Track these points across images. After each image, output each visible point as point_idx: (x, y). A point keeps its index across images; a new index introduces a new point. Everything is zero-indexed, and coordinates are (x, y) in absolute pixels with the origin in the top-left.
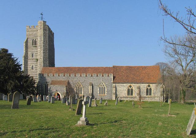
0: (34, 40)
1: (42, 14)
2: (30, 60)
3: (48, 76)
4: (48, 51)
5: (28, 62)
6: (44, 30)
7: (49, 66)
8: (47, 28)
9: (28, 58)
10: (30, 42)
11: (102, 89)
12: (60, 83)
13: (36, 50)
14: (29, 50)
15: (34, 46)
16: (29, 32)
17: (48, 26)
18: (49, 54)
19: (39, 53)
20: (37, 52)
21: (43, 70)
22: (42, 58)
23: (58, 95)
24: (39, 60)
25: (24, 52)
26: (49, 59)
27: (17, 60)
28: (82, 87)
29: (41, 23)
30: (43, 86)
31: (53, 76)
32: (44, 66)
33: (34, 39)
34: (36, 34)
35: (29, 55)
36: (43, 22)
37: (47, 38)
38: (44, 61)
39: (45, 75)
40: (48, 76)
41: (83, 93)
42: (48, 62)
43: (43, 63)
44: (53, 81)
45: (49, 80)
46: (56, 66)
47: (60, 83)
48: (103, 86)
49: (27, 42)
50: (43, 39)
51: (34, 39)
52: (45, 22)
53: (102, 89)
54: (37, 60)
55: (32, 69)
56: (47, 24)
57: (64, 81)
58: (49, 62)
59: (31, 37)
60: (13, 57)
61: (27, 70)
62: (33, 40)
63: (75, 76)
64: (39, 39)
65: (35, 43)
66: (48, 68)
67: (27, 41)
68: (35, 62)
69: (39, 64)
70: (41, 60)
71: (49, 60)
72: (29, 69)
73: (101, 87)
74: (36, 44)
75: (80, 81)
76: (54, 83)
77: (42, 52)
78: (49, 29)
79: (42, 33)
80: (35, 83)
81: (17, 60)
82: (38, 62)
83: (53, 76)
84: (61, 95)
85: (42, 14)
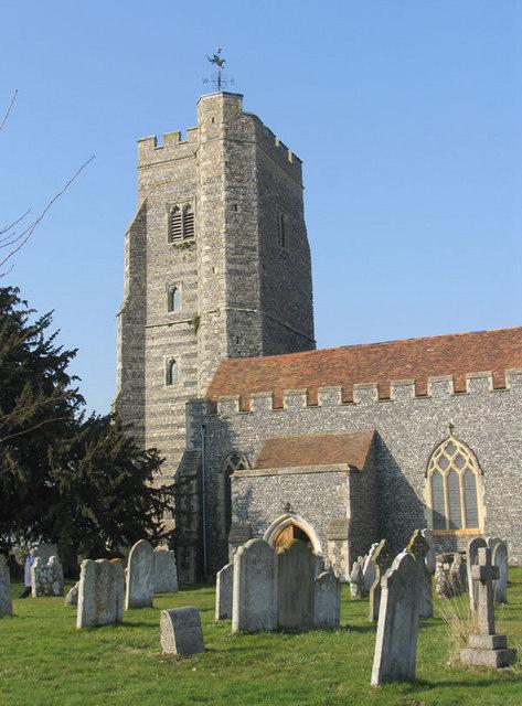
0: (181, 212)
1: (217, 61)
2: (157, 330)
3: (244, 411)
4: (256, 264)
5: (149, 343)
6: (233, 140)
7: (268, 352)
8: (250, 132)
9: (144, 321)
10: (159, 224)
11: (452, 490)
12: (315, 452)
13: (188, 267)
14: (151, 270)
15: (178, 242)
16: (149, 173)
17: (255, 118)
18: (263, 280)
19: (204, 279)
20: (194, 278)
21: (222, 381)
22: (222, 306)
23: (300, 535)
24: (203, 321)
25: (127, 281)
26: (264, 305)
27: (44, 323)
28: (475, 470)
29: (211, 106)
30: (216, 483)
31: (278, 407)
32: (234, 353)
33: (181, 206)
34: (190, 174)
35: (149, 302)
36: (221, 101)
37: (252, 185)
38: (233, 322)
39: (228, 409)
40: (244, 411)
41: (482, 513)
42: (257, 326)
43: (224, 336)
44: (270, 443)
45: (248, 437)
46: (320, 346)
47: (315, 452)
48: (459, 460)
49: (139, 229)
50: (223, 195)
51: (181, 206)
52: (233, 98)
53: (452, 490)
54: (196, 321)
55: (170, 382)
56: (247, 106)
57: (345, 440)
58: (267, 328)
59: (164, 196)
60: (17, 308)
61: (141, 389)
62: (177, 209)
63: (421, 395)
64: (204, 198)
65: (182, 225)
66: (265, 362)
67: (142, 219)
68: (187, 338)
69: (204, 343)
70: (216, 322)
71: (267, 317)
72: (150, 382)
73: (459, 472)
74: (188, 232)
75: (458, 430)
76: (276, 455)
77: (222, 268)
78: (265, 136)
79: (220, 161)
80: (155, 463)
81: (44, 323)
82: (202, 331)
83: (278, 407)
84: (320, 535)
85: (217, 61)
